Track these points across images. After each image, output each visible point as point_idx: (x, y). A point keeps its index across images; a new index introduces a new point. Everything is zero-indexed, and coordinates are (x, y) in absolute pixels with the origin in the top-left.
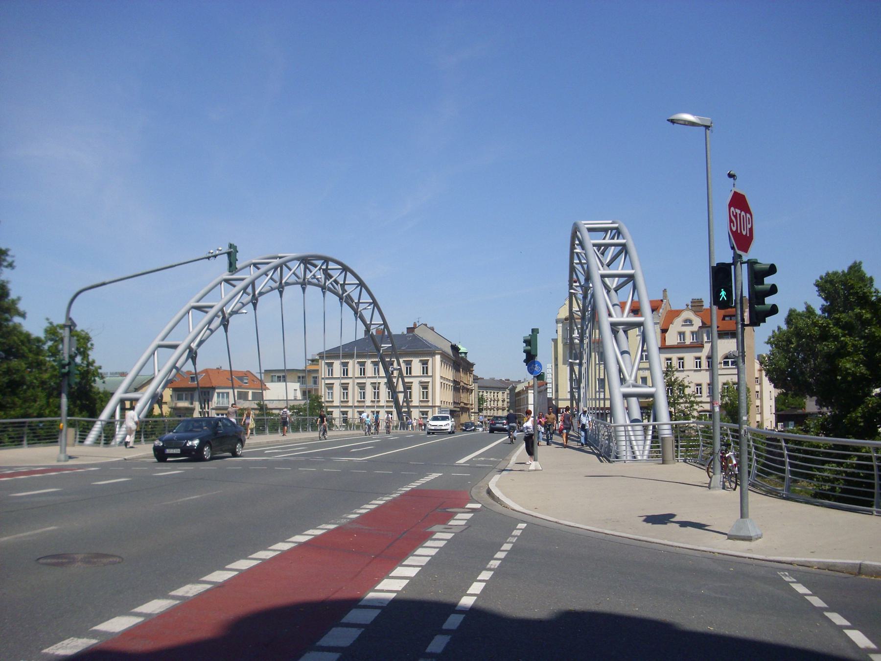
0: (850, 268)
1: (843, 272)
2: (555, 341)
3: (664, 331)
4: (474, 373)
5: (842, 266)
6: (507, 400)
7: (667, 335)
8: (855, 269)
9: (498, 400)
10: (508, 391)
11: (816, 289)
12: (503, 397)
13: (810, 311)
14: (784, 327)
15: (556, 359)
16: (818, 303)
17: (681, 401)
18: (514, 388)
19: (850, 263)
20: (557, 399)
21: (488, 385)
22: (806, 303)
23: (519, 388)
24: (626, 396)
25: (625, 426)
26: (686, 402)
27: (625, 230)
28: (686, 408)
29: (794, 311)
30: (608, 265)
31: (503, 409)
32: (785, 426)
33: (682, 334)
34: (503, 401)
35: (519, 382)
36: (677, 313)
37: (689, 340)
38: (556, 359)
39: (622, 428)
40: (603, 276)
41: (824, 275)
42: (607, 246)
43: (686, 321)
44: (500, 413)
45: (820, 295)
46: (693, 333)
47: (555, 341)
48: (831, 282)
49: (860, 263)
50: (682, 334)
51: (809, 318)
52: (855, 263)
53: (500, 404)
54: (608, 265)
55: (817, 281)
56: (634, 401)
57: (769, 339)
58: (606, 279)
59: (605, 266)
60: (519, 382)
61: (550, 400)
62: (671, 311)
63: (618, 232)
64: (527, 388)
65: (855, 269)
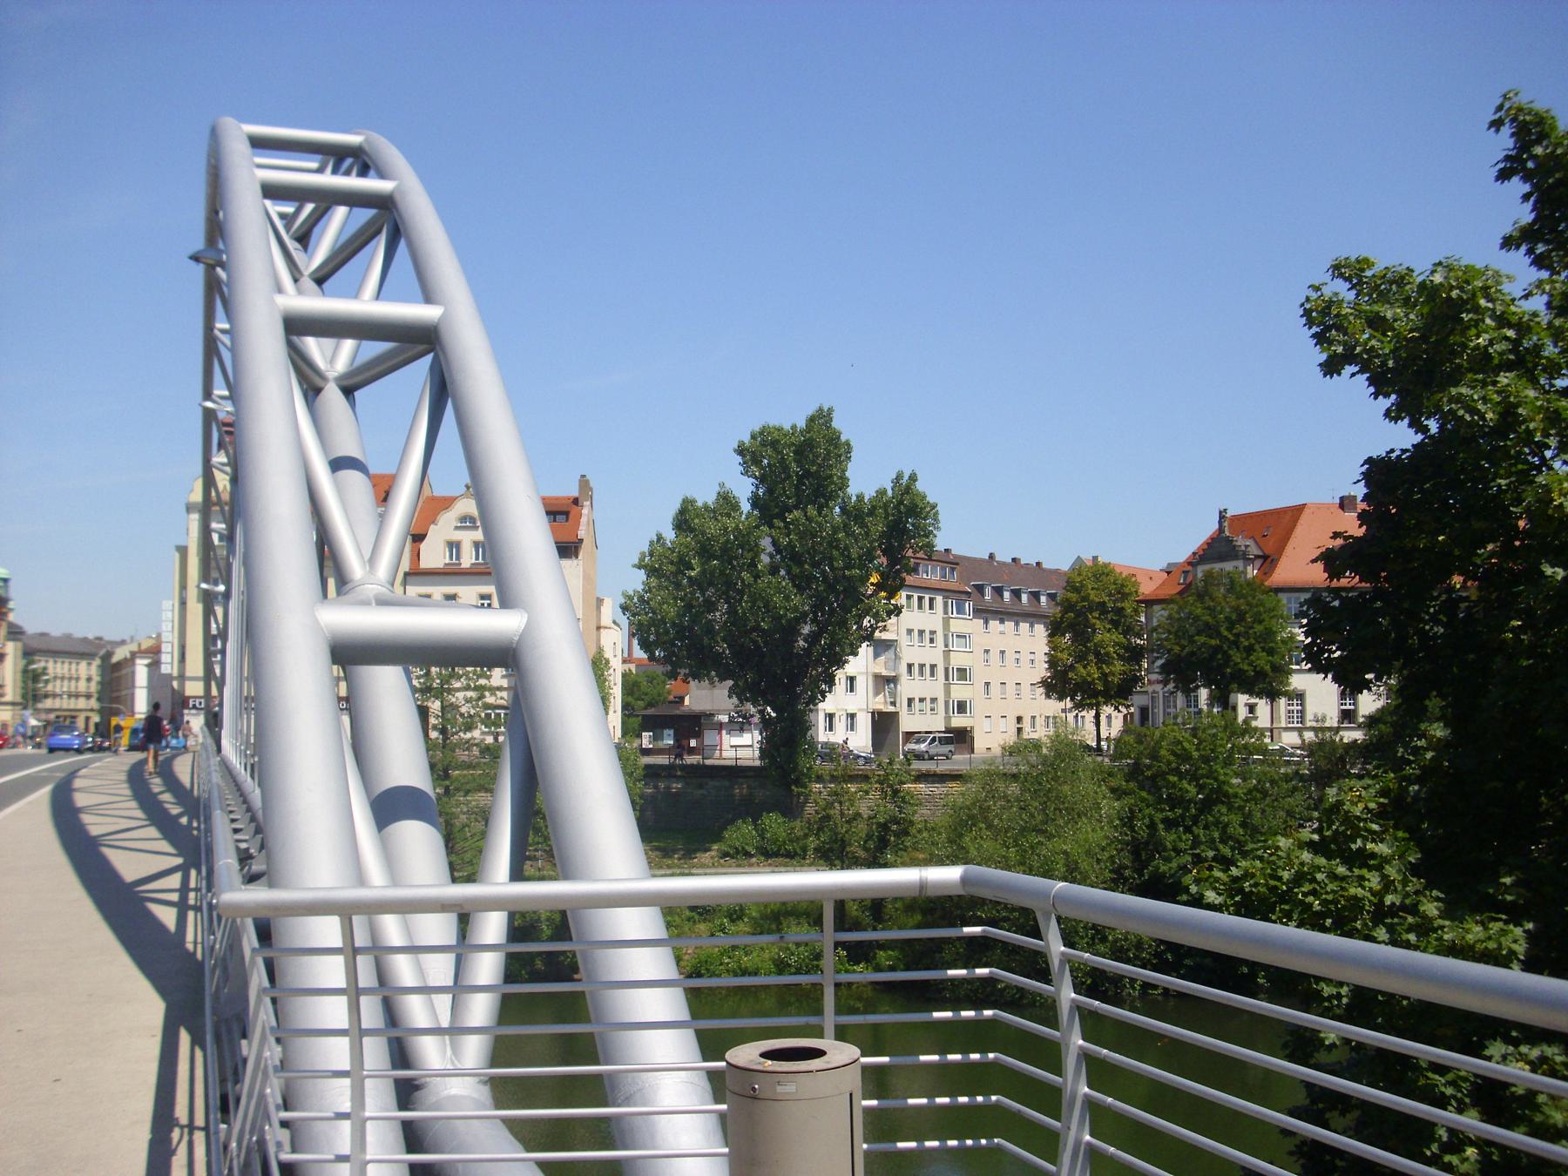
0: (811, 420)
1: (794, 427)
2: (183, 551)
3: (418, 538)
4: (11, 617)
5: (791, 416)
6: (96, 678)
7: (423, 546)
8: (821, 419)
9: (78, 679)
10: (97, 662)
11: (739, 459)
12: (87, 673)
13: (727, 501)
14: (670, 535)
15: (183, 587)
16: (744, 489)
17: (458, 685)
18: (109, 655)
19: (811, 410)
20: (182, 677)
21: (60, 647)
22: (722, 485)
23: (120, 654)
24: (350, 655)
25: (345, 911)
26: (468, 688)
27: (390, 154)
28: (468, 701)
29: (693, 502)
30: (320, 279)
31: (88, 696)
32: (655, 738)
33: (454, 546)
34: (89, 680)
35: (123, 642)
36: (447, 503)
37: (468, 559)
38: (183, 587)
39: (327, 931)
40: (296, 326)
41: (747, 439)
42: (327, 199)
43: (463, 519)
44: (82, 703)
45: (746, 473)
46: (476, 545)
47: (183, 551)
48: (774, 444)
49: (830, 410)
50: (454, 546)
51: (728, 515)
52: (821, 409)
53: (82, 686)
54: (320, 279)
55: (741, 444)
56: (388, 687)
57: (642, 559)
58: (313, 346)
59: (308, 283)
60: (123, 642)
61: (170, 677)
62: (433, 499)
63: (362, 161)
64: (134, 655)
65: (821, 419)
